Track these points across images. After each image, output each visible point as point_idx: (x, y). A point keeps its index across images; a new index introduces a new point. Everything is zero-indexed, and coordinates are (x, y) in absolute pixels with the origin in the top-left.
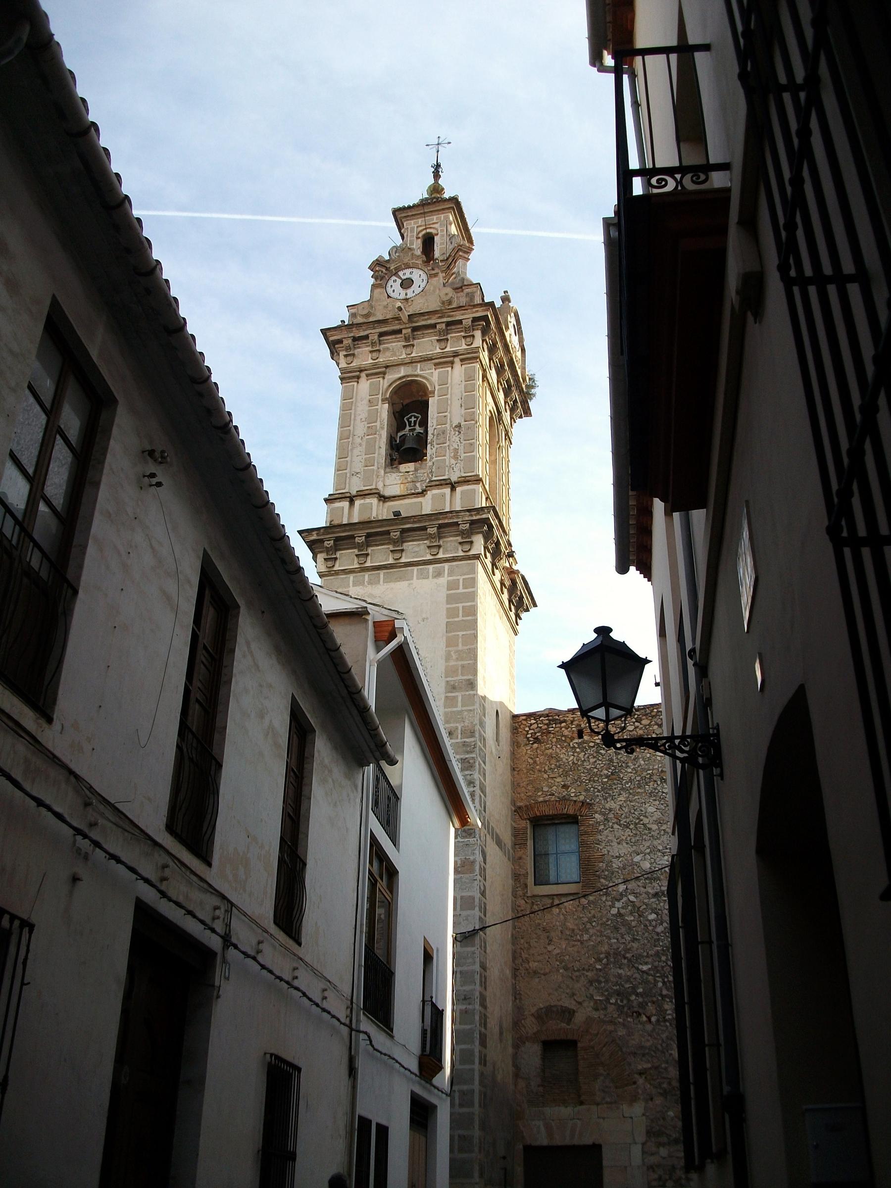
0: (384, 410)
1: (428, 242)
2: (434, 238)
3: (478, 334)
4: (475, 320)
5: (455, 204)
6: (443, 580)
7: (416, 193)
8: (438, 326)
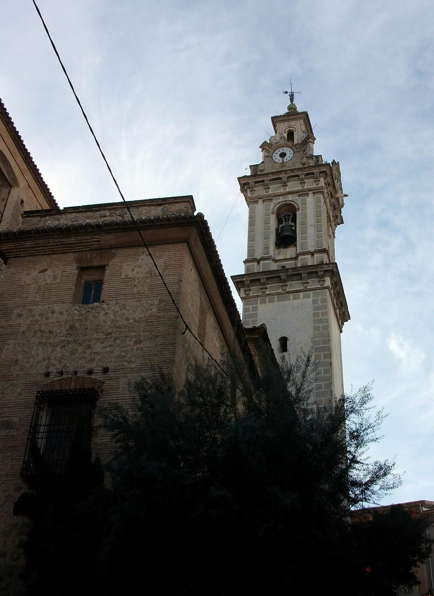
0: (273, 219)
1: (291, 135)
3: (322, 179)
4: (321, 172)
5: (305, 116)
6: (310, 300)
7: (284, 111)
8: (265, 182)
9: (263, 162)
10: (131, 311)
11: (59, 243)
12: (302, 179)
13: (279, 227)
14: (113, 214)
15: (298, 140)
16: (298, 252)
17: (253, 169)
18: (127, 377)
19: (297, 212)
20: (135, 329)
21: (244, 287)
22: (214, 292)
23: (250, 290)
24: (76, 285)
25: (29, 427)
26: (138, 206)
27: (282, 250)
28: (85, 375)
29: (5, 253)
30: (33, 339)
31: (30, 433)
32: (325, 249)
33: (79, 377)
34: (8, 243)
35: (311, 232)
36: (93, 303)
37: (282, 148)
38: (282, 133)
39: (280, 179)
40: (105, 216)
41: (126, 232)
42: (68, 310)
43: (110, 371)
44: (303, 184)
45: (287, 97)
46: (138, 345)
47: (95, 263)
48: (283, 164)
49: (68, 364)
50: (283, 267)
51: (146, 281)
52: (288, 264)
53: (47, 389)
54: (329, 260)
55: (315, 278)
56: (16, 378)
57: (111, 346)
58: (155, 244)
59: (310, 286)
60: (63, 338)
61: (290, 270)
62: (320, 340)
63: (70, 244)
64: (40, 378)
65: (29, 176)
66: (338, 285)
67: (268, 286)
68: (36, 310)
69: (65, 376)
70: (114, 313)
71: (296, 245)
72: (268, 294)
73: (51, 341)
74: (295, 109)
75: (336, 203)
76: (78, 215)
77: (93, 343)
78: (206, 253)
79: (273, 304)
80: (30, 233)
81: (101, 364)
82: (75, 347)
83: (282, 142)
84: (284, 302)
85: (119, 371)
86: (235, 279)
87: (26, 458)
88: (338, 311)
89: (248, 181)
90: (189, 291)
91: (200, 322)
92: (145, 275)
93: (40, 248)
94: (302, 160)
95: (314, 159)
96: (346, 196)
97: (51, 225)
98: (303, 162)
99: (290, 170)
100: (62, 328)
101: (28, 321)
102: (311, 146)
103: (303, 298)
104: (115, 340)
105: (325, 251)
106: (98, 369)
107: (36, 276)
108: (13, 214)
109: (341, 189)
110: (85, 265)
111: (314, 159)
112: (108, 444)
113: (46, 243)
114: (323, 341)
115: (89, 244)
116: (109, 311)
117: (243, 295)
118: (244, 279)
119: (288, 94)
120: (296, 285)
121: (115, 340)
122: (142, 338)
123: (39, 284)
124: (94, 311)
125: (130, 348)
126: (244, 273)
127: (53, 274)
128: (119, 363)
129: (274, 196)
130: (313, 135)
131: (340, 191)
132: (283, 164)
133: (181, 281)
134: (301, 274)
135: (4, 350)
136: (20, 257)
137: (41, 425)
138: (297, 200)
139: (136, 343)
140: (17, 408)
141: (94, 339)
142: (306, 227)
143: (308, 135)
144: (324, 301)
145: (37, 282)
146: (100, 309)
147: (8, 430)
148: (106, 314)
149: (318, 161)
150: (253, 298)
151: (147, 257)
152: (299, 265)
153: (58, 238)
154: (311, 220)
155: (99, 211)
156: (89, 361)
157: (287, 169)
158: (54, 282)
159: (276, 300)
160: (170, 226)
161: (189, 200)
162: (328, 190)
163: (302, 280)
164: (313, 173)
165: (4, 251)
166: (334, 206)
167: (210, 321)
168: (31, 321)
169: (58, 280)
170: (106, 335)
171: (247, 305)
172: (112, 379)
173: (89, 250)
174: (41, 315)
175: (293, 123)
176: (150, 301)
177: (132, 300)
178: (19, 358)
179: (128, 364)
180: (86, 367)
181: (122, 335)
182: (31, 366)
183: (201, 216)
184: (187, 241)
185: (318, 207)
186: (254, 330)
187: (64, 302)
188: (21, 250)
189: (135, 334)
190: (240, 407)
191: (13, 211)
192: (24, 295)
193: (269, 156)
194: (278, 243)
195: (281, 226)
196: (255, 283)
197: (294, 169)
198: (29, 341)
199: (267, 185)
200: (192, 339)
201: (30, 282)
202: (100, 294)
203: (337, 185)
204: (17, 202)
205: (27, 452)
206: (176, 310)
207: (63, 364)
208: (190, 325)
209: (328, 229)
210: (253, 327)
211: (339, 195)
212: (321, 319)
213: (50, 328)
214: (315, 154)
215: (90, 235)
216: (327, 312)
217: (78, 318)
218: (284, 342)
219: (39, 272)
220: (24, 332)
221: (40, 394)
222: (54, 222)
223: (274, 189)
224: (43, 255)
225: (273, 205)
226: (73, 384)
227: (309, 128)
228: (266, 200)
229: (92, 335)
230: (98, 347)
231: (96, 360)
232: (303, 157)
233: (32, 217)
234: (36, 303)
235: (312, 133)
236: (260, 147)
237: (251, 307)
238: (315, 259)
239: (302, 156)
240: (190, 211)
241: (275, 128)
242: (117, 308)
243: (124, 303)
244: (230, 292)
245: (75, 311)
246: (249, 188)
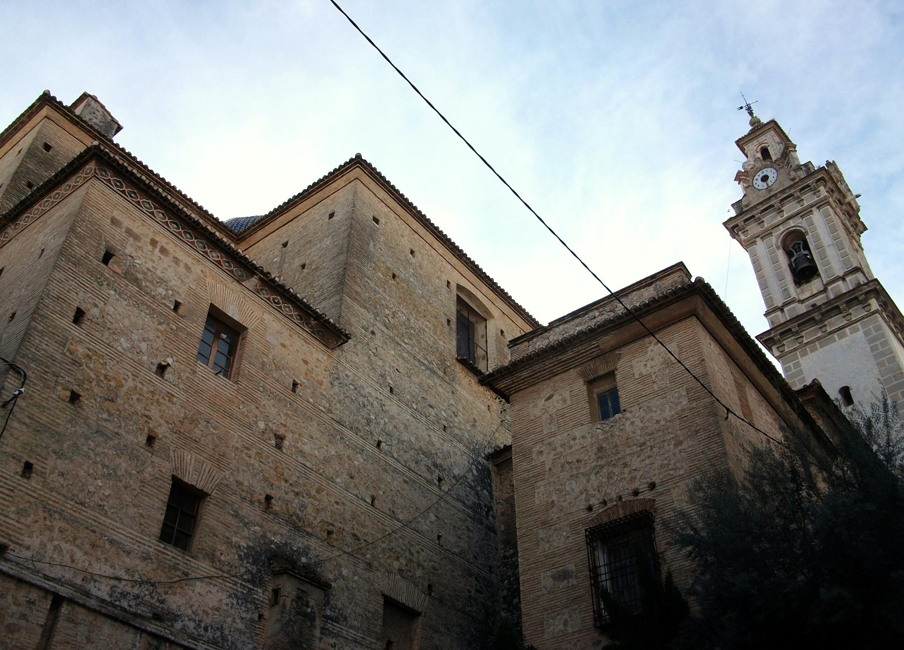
0: (781, 255)
1: (765, 152)
2: (767, 149)
3: (822, 188)
5: (774, 125)
6: (860, 334)
7: (746, 129)
9: (745, 196)
10: (659, 412)
11: (557, 363)
12: (798, 197)
13: (791, 261)
14: (603, 313)
15: (776, 154)
16: (825, 283)
17: (737, 207)
18: (678, 487)
19: (807, 237)
20: (670, 430)
21: (775, 344)
22: (744, 360)
23: (784, 345)
24: (590, 402)
25: (588, 572)
26: (626, 294)
27: (805, 286)
28: (632, 498)
29: (505, 391)
30: (562, 474)
31: (591, 578)
32: (856, 267)
33: (625, 502)
35: (832, 254)
36: (614, 415)
37: (761, 171)
38: (755, 155)
39: (772, 206)
40: (595, 317)
42: (589, 431)
43: (657, 485)
44: (801, 203)
45: (744, 112)
46: (680, 448)
47: (602, 372)
48: (769, 188)
49: (609, 491)
50: (814, 305)
51: (664, 373)
52: (818, 300)
53: (595, 524)
54: (867, 279)
55: (857, 305)
56: (558, 522)
57: (649, 457)
58: (660, 329)
59: (855, 317)
60: (593, 464)
61: (823, 307)
62: (890, 377)
64: (584, 515)
65: (500, 303)
66: (888, 304)
67: (803, 334)
68: (555, 442)
69: (609, 505)
70: (640, 419)
71: (819, 275)
72: (806, 344)
73: (582, 470)
74: (759, 121)
75: (849, 208)
76: (566, 326)
77: (627, 460)
78: (720, 320)
79: (817, 352)
80: (523, 362)
81: (645, 481)
82: (610, 470)
83: (759, 165)
84: (829, 346)
85: (668, 483)
86: (761, 338)
87: (595, 606)
88: (899, 335)
89: (736, 223)
90: (716, 368)
91: (741, 400)
92: (660, 367)
94: (789, 175)
95: (804, 168)
96: (858, 196)
97: (541, 346)
98: (792, 177)
99: (780, 192)
100: (590, 453)
101: (551, 456)
102: (794, 156)
103: (851, 334)
104: (651, 449)
105: (857, 270)
106: (643, 487)
107: (544, 405)
108: (496, 348)
109: (849, 190)
110: (591, 377)
111: (804, 168)
112: (681, 569)
114: (894, 376)
115: (588, 353)
116: (634, 419)
117: (777, 354)
118: (772, 335)
119: (744, 108)
120: (836, 321)
121: (651, 449)
122: (681, 438)
123: (550, 413)
124: (618, 424)
125: (671, 453)
126: (769, 328)
127: (560, 397)
128: (664, 474)
129: (772, 229)
130: (791, 142)
131: (848, 194)
132: (769, 189)
133: (703, 360)
134: (838, 307)
135: (536, 494)
136: (521, 390)
137: (600, 567)
138: (801, 223)
139: (676, 446)
140: (568, 554)
141: (628, 455)
142: (824, 250)
143: (786, 144)
144: (879, 328)
145: (547, 412)
146: (624, 420)
147: (566, 581)
148: (632, 423)
149: (809, 169)
150: (789, 353)
151: (656, 347)
152: (832, 297)
153: (554, 357)
154: (826, 239)
155: (586, 314)
156: (631, 480)
157: (776, 192)
158: (566, 406)
159: (818, 346)
161: (680, 267)
162: (834, 197)
163: (841, 313)
164: (808, 185)
166: (848, 213)
167: (752, 395)
168: (555, 455)
169: (569, 402)
170: (640, 446)
171: (786, 364)
172: (663, 494)
173: (590, 360)
174: (563, 445)
175: (762, 139)
176: (676, 394)
177: (655, 399)
178: (554, 499)
179: (675, 472)
180: (630, 488)
181: (658, 441)
182: (570, 503)
183: (700, 280)
184: (694, 314)
185: (829, 222)
186: (806, 389)
187: (582, 425)
188: (520, 382)
189: (672, 436)
190: (822, 486)
191: (496, 345)
194: (797, 280)
195: (793, 259)
196: (785, 336)
197: (784, 190)
198: (558, 477)
199: (759, 219)
200: (738, 423)
201: (540, 413)
202: (618, 403)
203: (842, 187)
204: (497, 334)
205: (595, 600)
206: (710, 395)
207: (604, 493)
208: (730, 406)
209: (851, 243)
210: (804, 386)
211: (849, 199)
212: (882, 352)
213: (577, 457)
214: (802, 162)
216: (886, 340)
217: (603, 437)
218: (845, 392)
219: (546, 400)
220: (550, 469)
221: (589, 532)
222: (543, 343)
223: (770, 220)
224: (544, 380)
225: (775, 239)
226: (621, 511)
227: (783, 137)
228: (765, 236)
229: (624, 451)
230: (635, 463)
231: (638, 477)
232: (789, 172)
233: (518, 344)
234: (553, 435)
235: (789, 141)
236: (735, 180)
237: (791, 364)
238: (849, 282)
239: (787, 171)
240: (686, 279)
241: (743, 152)
242: (642, 413)
243: (648, 405)
244: (764, 355)
245: (598, 430)
246: (740, 230)
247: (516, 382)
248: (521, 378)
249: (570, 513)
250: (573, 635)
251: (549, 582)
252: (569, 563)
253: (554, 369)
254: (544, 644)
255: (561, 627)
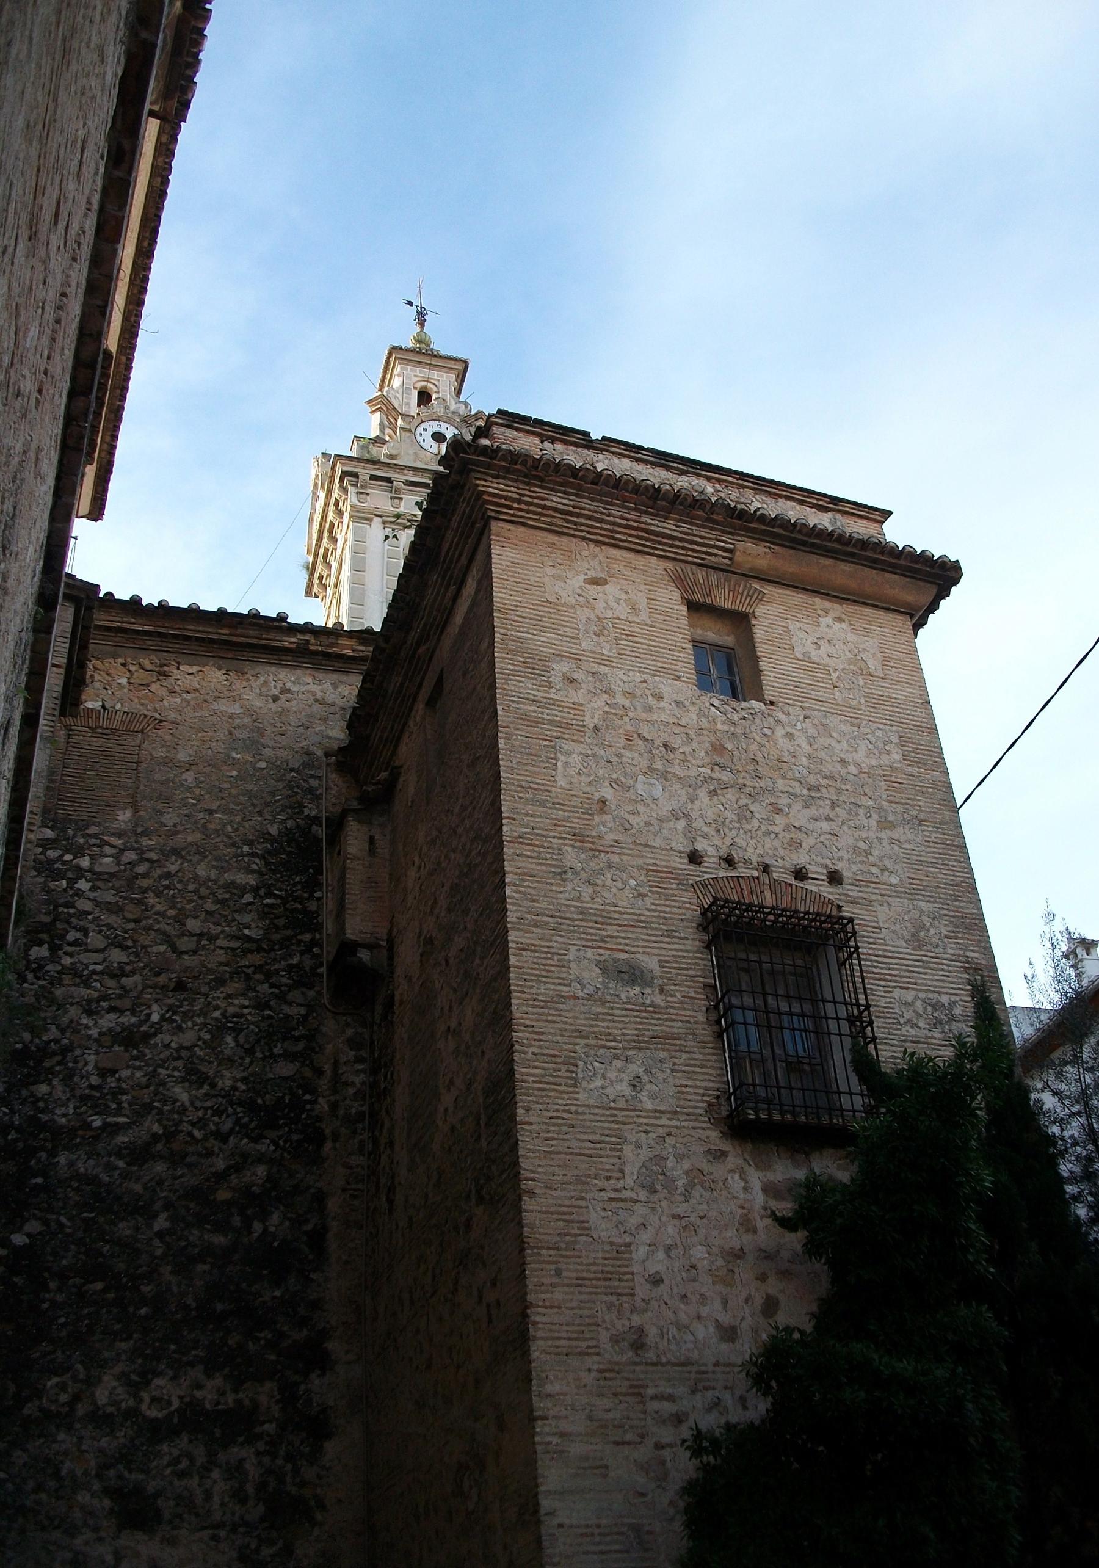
11: (635, 524)
34: (502, 481)
41: (794, 549)
63: (659, 534)
85: (868, 887)
89: (356, 470)
93: (583, 521)
113: (602, 513)
115: (704, 549)
136: (524, 525)
147: (637, 989)
153: (635, 509)
155: (682, 473)
160: (892, 569)
165: (486, 497)
175: (435, 374)
192: (567, 629)
193: (409, 430)
215: (712, 529)
224: (584, 538)
233: (517, 429)
247: (526, 503)
248: (542, 502)
249: (647, 846)
250: (656, 1118)
251: (593, 976)
252: (644, 953)
253: (619, 533)
254: (576, 1113)
255: (624, 1088)
